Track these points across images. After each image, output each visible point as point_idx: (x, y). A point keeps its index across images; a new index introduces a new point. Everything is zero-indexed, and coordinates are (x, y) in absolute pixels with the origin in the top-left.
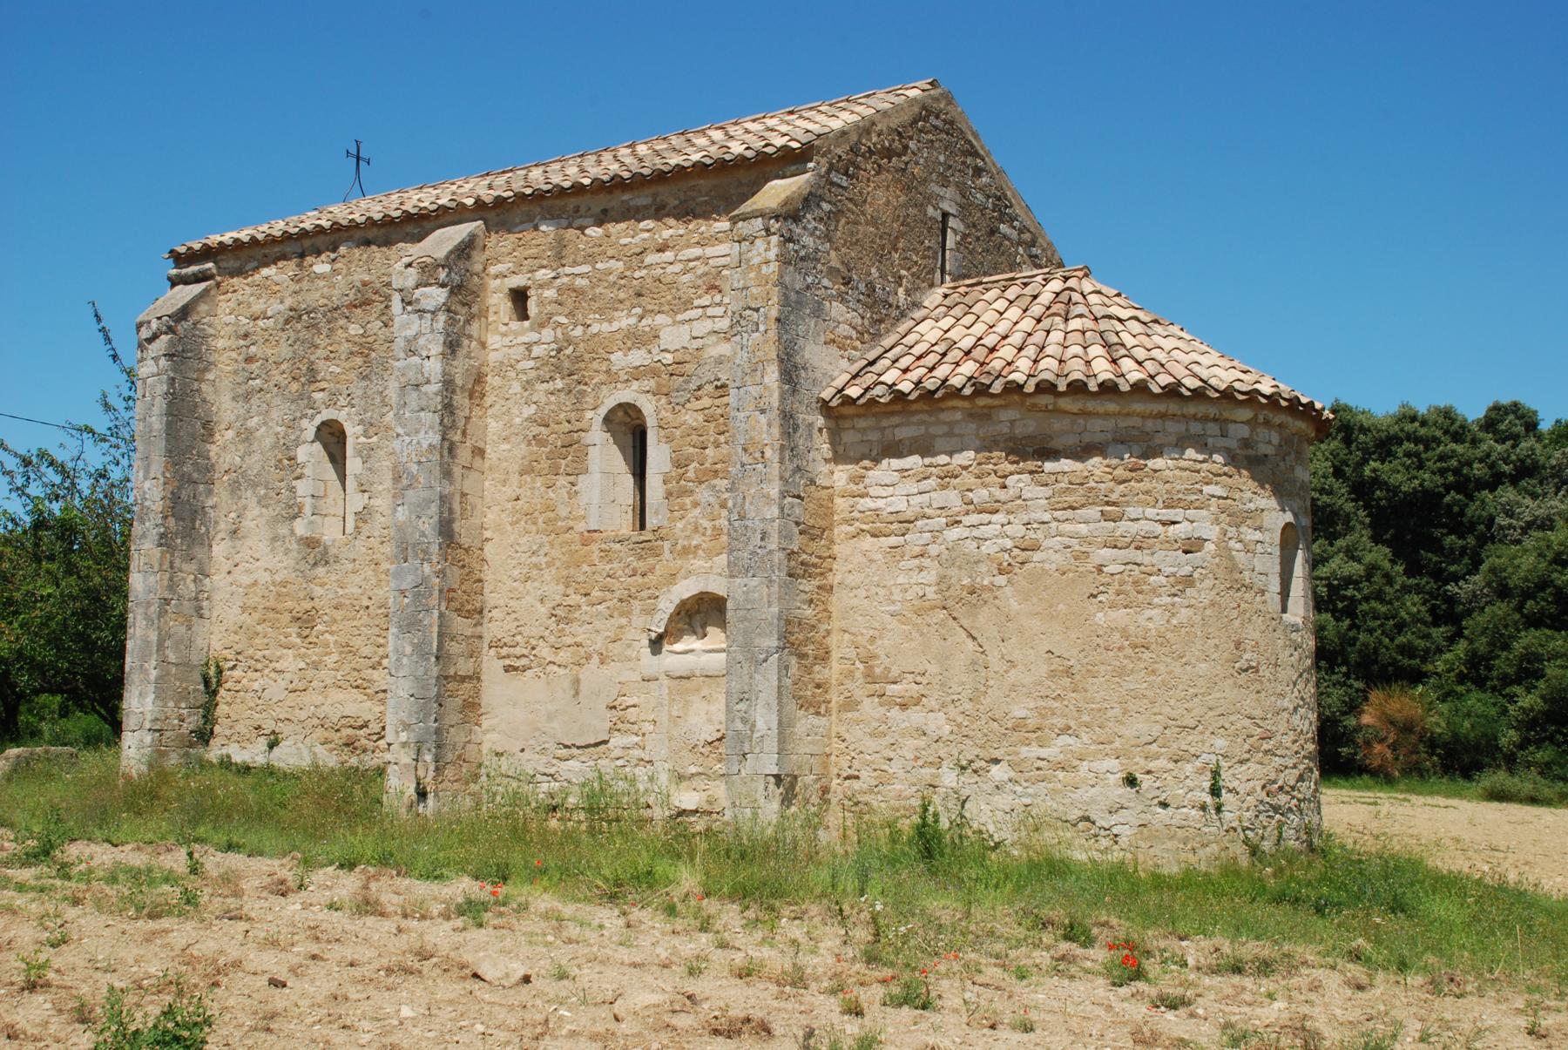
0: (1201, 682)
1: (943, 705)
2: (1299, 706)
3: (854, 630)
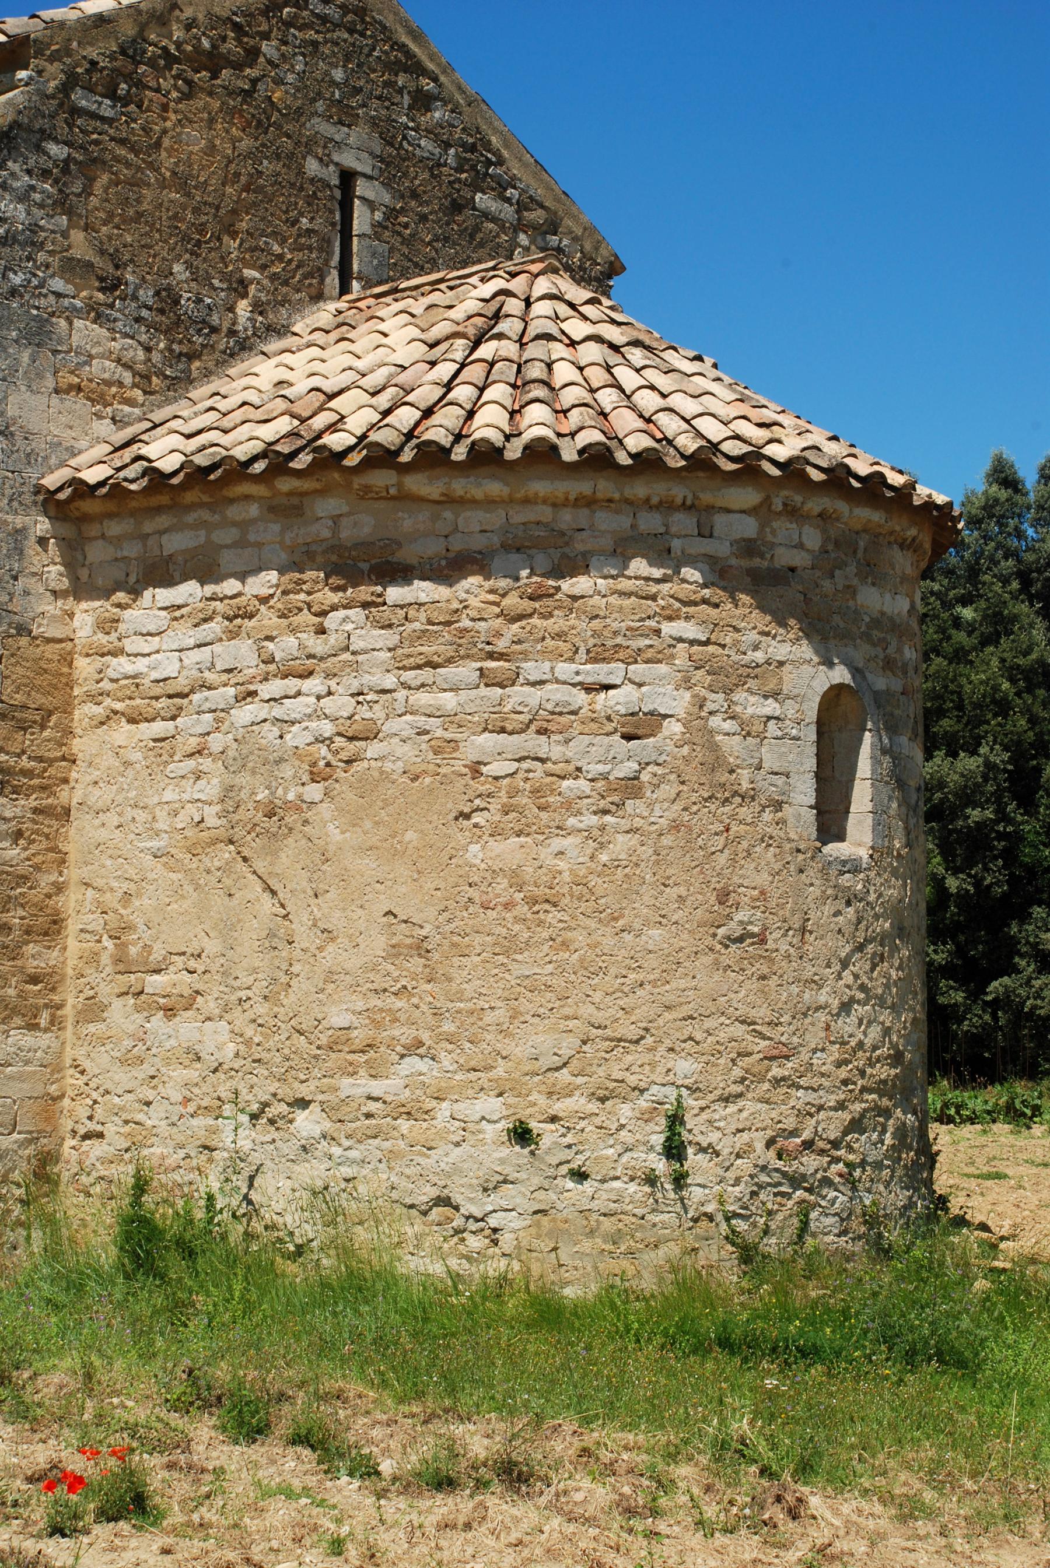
0: (651, 961)
1: (226, 1009)
2: (852, 1000)
3: (99, 883)
